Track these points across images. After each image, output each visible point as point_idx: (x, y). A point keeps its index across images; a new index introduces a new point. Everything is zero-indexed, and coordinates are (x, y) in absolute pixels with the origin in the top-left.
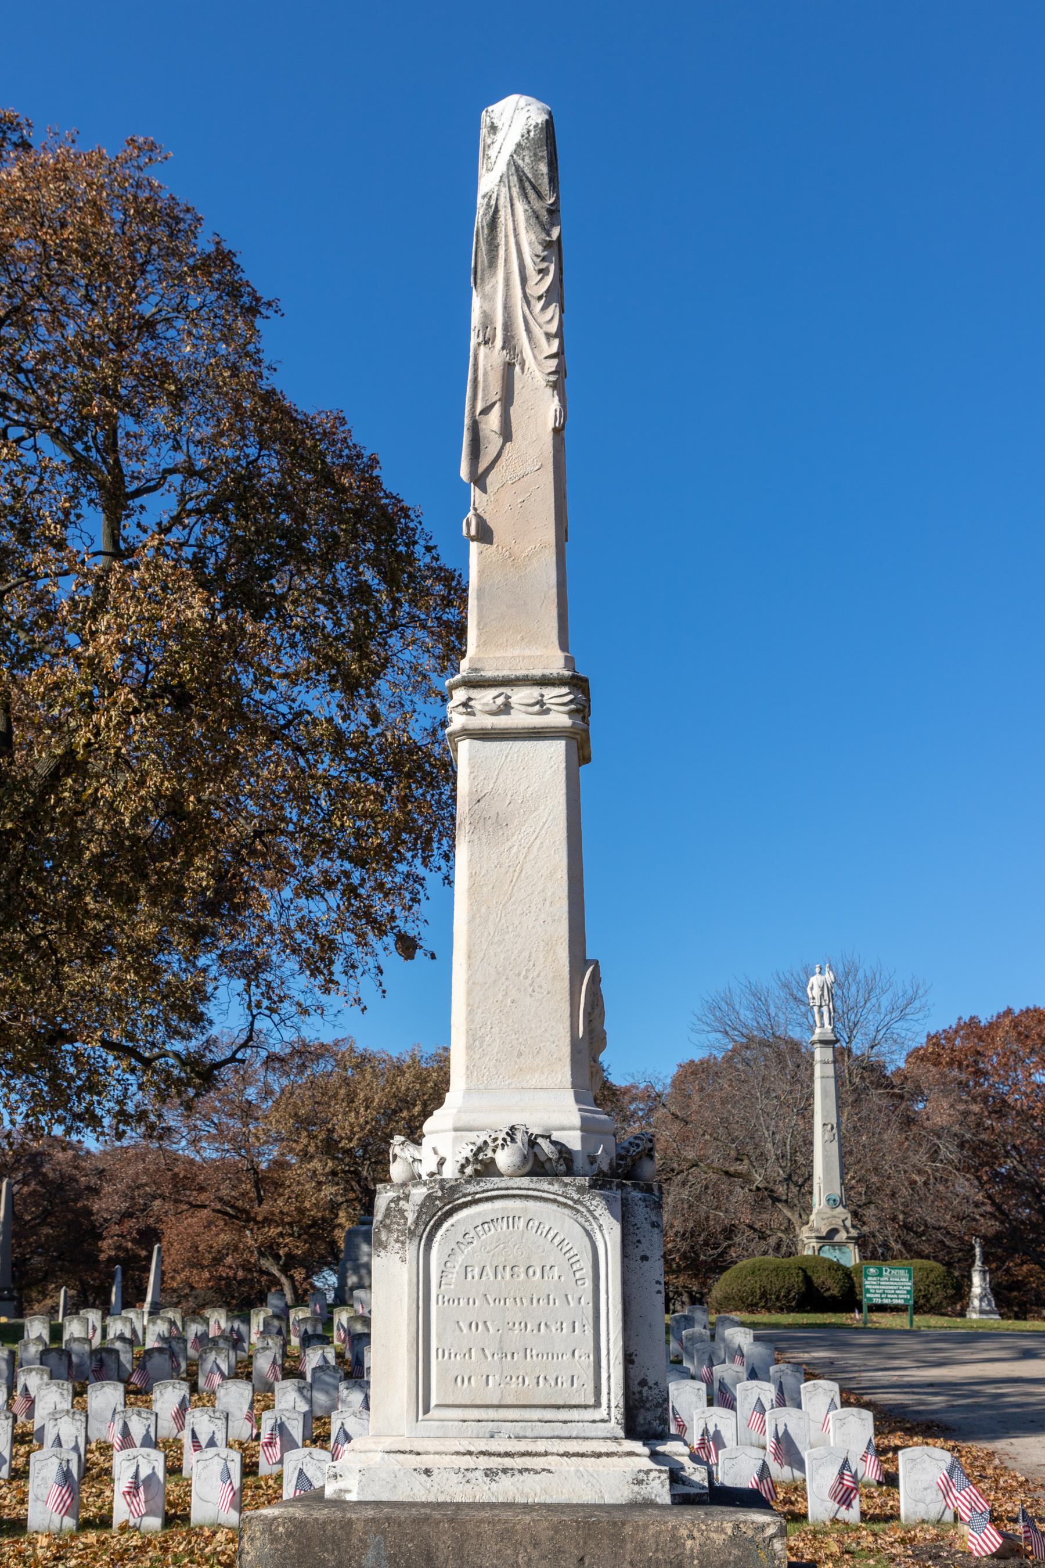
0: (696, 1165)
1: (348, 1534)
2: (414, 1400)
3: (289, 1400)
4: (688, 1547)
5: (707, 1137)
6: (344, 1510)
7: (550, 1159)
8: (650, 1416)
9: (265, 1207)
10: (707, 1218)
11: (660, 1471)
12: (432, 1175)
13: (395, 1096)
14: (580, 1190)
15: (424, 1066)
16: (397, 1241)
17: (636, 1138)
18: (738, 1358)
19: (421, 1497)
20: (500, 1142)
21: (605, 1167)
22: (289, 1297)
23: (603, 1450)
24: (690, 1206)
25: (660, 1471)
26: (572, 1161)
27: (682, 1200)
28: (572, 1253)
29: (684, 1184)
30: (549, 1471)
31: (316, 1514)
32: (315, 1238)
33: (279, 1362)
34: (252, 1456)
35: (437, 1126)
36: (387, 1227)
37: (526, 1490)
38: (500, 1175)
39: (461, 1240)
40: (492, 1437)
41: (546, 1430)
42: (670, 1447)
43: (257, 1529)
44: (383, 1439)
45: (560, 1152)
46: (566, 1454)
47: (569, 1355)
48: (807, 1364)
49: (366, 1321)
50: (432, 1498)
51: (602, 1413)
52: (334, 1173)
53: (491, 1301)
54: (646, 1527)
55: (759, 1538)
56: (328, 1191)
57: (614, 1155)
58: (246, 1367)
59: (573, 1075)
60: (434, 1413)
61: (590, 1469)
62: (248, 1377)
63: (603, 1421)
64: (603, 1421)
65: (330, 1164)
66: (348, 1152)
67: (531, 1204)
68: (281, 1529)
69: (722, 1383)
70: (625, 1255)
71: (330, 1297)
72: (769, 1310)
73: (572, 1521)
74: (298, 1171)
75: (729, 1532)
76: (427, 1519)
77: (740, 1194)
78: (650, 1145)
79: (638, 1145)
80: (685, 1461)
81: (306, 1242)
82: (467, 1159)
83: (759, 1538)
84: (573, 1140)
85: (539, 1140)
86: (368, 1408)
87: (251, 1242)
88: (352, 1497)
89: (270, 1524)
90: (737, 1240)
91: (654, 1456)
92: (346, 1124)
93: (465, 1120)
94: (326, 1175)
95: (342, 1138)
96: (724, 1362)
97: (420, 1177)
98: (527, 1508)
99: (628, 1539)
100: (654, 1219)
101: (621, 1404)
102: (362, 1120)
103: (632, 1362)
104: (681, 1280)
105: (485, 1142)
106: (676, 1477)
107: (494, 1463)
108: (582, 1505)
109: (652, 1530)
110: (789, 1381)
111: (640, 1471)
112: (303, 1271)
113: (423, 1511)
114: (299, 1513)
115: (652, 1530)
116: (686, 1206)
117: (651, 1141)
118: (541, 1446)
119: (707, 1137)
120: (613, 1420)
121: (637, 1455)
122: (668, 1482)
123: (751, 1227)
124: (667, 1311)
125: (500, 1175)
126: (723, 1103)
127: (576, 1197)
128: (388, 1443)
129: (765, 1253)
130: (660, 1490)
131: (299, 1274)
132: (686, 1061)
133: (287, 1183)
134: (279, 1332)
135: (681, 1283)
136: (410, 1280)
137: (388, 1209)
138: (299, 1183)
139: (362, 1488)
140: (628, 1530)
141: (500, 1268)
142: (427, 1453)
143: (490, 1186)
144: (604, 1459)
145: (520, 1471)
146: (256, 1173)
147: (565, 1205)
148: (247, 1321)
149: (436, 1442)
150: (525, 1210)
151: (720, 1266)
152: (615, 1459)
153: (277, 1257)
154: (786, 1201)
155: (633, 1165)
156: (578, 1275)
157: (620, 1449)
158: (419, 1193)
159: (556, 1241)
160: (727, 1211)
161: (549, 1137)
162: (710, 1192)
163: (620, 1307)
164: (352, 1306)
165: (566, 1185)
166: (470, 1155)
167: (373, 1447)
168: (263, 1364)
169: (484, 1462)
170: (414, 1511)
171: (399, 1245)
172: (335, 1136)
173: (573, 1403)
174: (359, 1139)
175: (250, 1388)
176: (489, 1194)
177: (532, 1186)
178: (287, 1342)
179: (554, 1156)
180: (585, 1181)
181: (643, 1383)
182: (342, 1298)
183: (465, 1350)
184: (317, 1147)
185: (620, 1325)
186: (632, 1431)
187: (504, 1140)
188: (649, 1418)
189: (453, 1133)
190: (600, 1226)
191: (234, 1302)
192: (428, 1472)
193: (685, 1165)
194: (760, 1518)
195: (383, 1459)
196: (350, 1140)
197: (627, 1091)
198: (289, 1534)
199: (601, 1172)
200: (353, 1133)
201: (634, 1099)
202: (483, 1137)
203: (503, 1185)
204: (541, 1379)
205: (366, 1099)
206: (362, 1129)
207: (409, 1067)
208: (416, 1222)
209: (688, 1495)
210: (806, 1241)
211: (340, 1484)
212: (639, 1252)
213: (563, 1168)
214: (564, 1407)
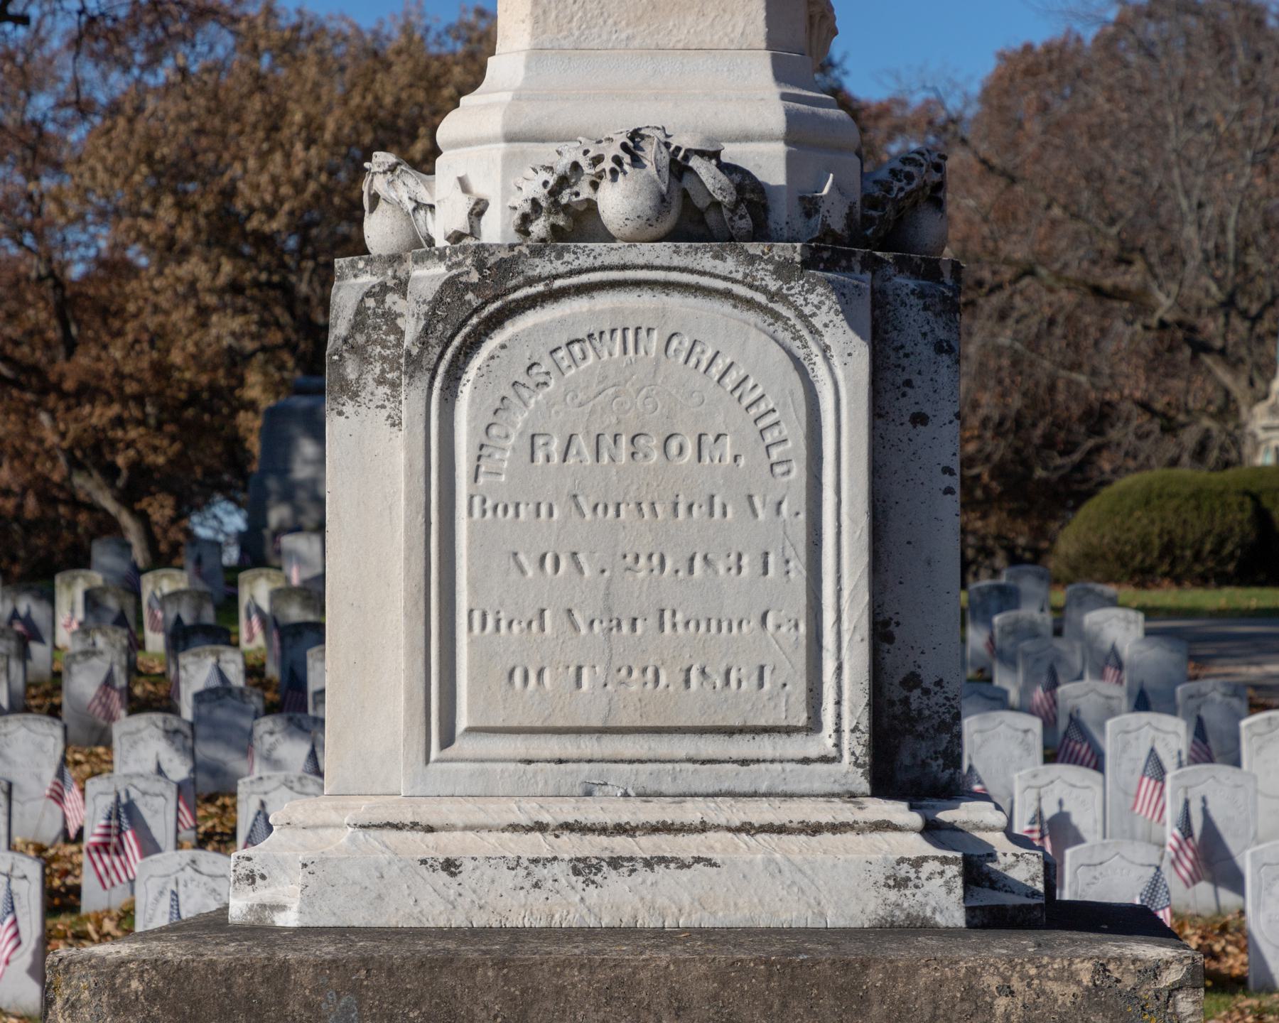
0: (1030, 272)
1: (280, 993)
2: (420, 718)
3: (144, 750)
4: (999, 1011)
5: (1057, 212)
6: (271, 944)
7: (717, 205)
8: (924, 749)
9: (83, 359)
10: (1052, 389)
11: (945, 861)
12: (457, 237)
13: (369, 118)
14: (783, 270)
15: (434, 49)
16: (381, 381)
17: (906, 160)
18: (1110, 672)
19: (436, 914)
20: (608, 165)
21: (838, 224)
22: (139, 554)
23: (825, 818)
24: (1015, 363)
25: (945, 861)
26: (765, 209)
27: (999, 351)
28: (762, 407)
29: (1003, 316)
30: (710, 863)
31: (210, 954)
32: (191, 433)
33: (121, 681)
34: (66, 873)
35: (469, 127)
36: (360, 353)
37: (661, 901)
38: (611, 238)
39: (522, 378)
40: (589, 794)
41: (705, 778)
42: (962, 814)
43: (83, 985)
44: (353, 802)
45: (740, 188)
46: (746, 828)
47: (755, 622)
48: (1257, 687)
49: (313, 593)
50: (459, 920)
51: (824, 742)
52: (235, 287)
53: (587, 510)
54: (912, 971)
55: (1147, 992)
56: (226, 328)
57: (857, 197)
58: (48, 694)
59: (769, 20)
60: (464, 746)
61: (798, 859)
62: (54, 712)
63: (825, 759)
64: (825, 759)
65: (227, 267)
66: (264, 240)
67: (675, 301)
68: (135, 984)
69: (1075, 720)
70: (878, 412)
71: (231, 555)
72: (1178, 581)
73: (758, 961)
74: (156, 286)
75: (1086, 979)
76: (448, 960)
77: (1125, 334)
78: (936, 177)
79: (910, 177)
80: (997, 840)
81: (173, 439)
82: (535, 202)
83: (1147, 992)
84: (769, 164)
85: (695, 162)
86: (319, 773)
87: (52, 439)
88: (288, 919)
89: (111, 973)
90: (1114, 434)
91: (932, 830)
92: (262, 181)
93: (531, 116)
94: (221, 292)
95: (251, 210)
96: (1080, 677)
97: (430, 241)
98: (662, 936)
99: (875, 997)
100: (942, 334)
101: (865, 724)
102: (298, 171)
103: (889, 638)
104: (991, 524)
105: (576, 166)
106: (977, 872)
107: (593, 846)
108: (779, 931)
109: (924, 977)
110: (1213, 716)
111: (901, 861)
112: (169, 501)
113: (440, 945)
114: (174, 952)
115: (924, 977)
116: (1005, 362)
117: (938, 168)
118: (692, 812)
119: (1057, 212)
120: (847, 757)
121: (897, 828)
122: (959, 881)
123: (1145, 406)
124: (964, 586)
125: (611, 238)
126: (1092, 138)
127: (773, 285)
128: (364, 809)
129: (1174, 462)
130: (942, 898)
131: (160, 509)
132: (1018, 45)
133: (131, 307)
134: (121, 621)
135: (992, 529)
136: (410, 465)
137: (360, 311)
138: (156, 309)
139: (309, 901)
140: (875, 977)
141: (607, 440)
142: (449, 828)
143: (584, 261)
144: (827, 837)
145: (648, 864)
146: (59, 284)
147: (750, 304)
148: (49, 597)
149: (469, 805)
150: (663, 314)
151: (1073, 491)
152: (850, 837)
153: (110, 472)
154: (1222, 352)
155: (899, 220)
156: (775, 453)
157: (860, 816)
158: (428, 277)
159: (729, 382)
160: (1094, 372)
161: (715, 155)
162: (1058, 331)
163: (864, 521)
164: (280, 568)
165: (752, 259)
166: (541, 193)
167: (334, 817)
168: (84, 684)
169: (571, 846)
170: (421, 946)
171: (385, 390)
172: (239, 206)
173: (762, 722)
174: (291, 213)
175: (58, 732)
176: (584, 278)
177: (677, 261)
178: (137, 644)
179: (726, 198)
180: (795, 251)
181: (912, 681)
182: (257, 550)
183: (531, 613)
184: (197, 230)
185: (865, 559)
186: (887, 777)
187: (617, 160)
188: (923, 754)
189: (503, 145)
190: (825, 350)
191: (17, 569)
192: (450, 866)
193: (1007, 273)
194: (1150, 951)
195: (353, 840)
196: (271, 213)
197: (883, 111)
198: (154, 995)
199: (828, 233)
200: (281, 201)
201: (898, 129)
202: (572, 153)
203: (614, 259)
204: (694, 674)
205: (309, 122)
206: (298, 187)
207: (399, 52)
208: (424, 339)
209: (1001, 908)
210: (1262, 435)
211: (263, 893)
212: (907, 406)
213: (745, 224)
214: (742, 730)
